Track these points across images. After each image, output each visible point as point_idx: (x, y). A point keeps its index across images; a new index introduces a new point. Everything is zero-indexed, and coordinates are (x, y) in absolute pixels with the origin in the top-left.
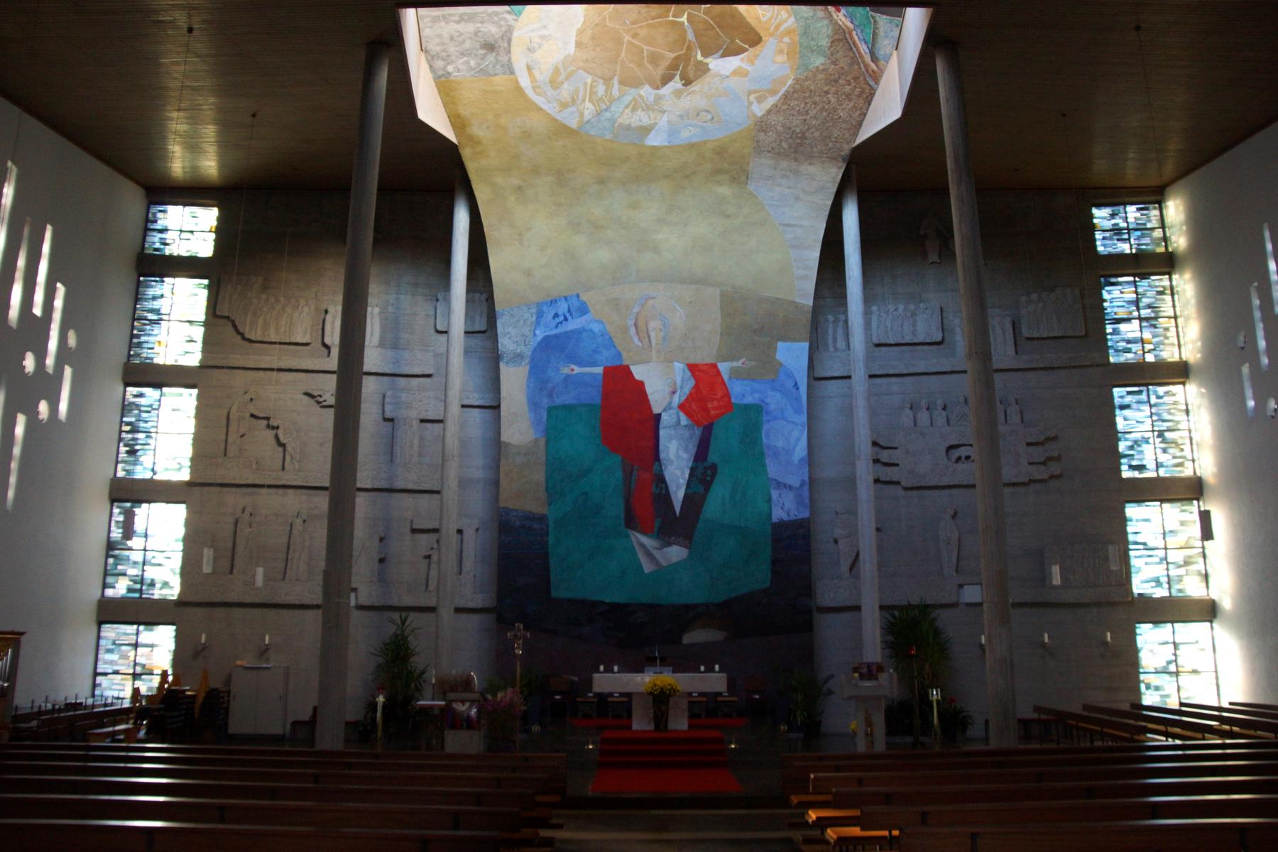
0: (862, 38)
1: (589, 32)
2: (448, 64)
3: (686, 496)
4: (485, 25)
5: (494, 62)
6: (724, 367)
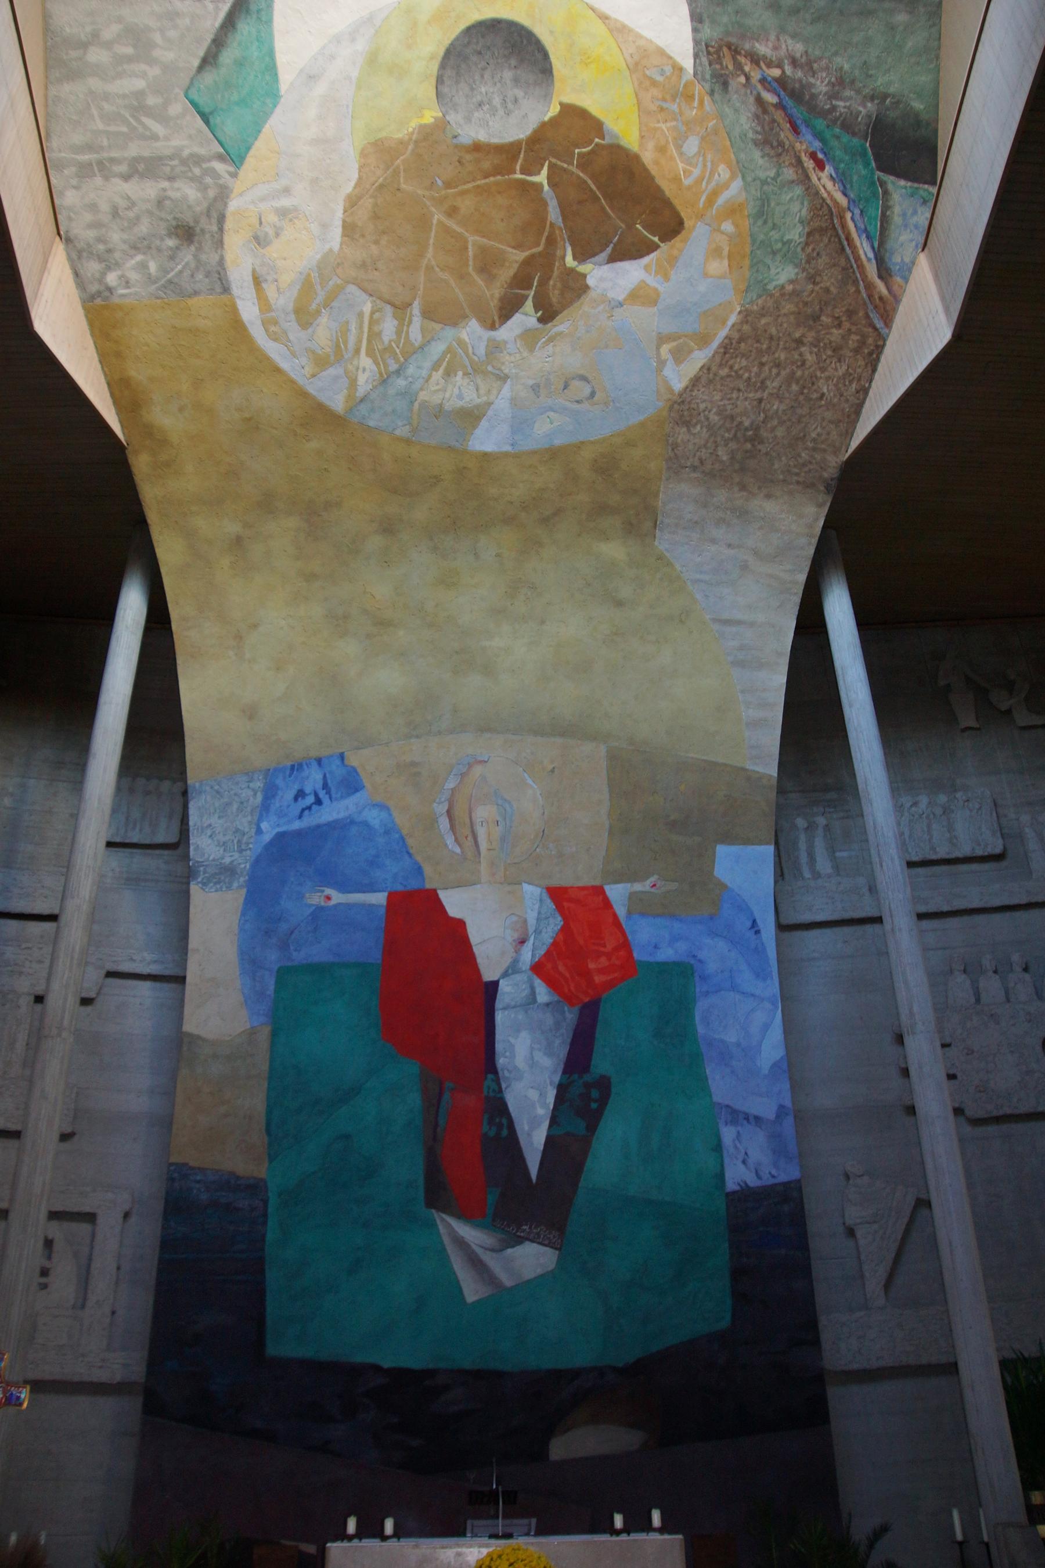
0: (863, 227)
1: (368, 202)
2: (109, 268)
3: (550, 1141)
4: (176, 185)
5: (193, 265)
6: (617, 893)
